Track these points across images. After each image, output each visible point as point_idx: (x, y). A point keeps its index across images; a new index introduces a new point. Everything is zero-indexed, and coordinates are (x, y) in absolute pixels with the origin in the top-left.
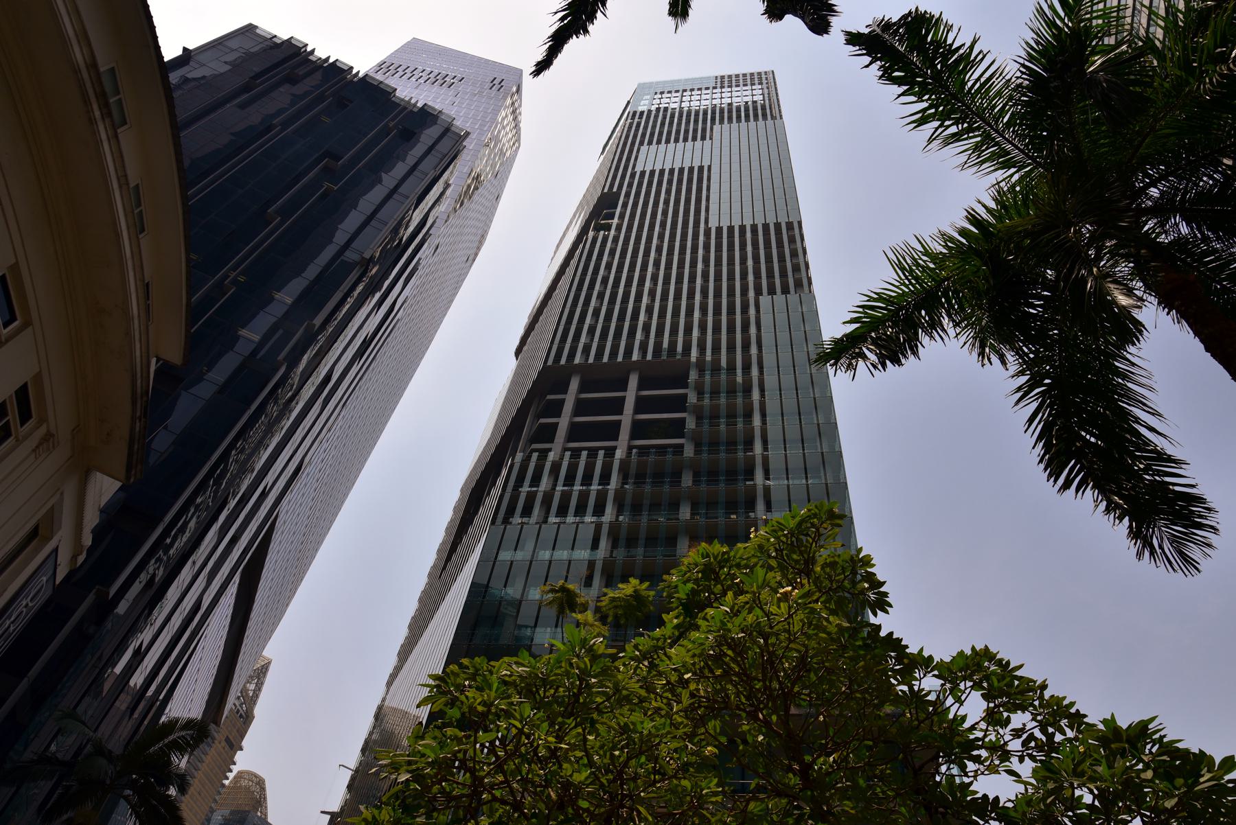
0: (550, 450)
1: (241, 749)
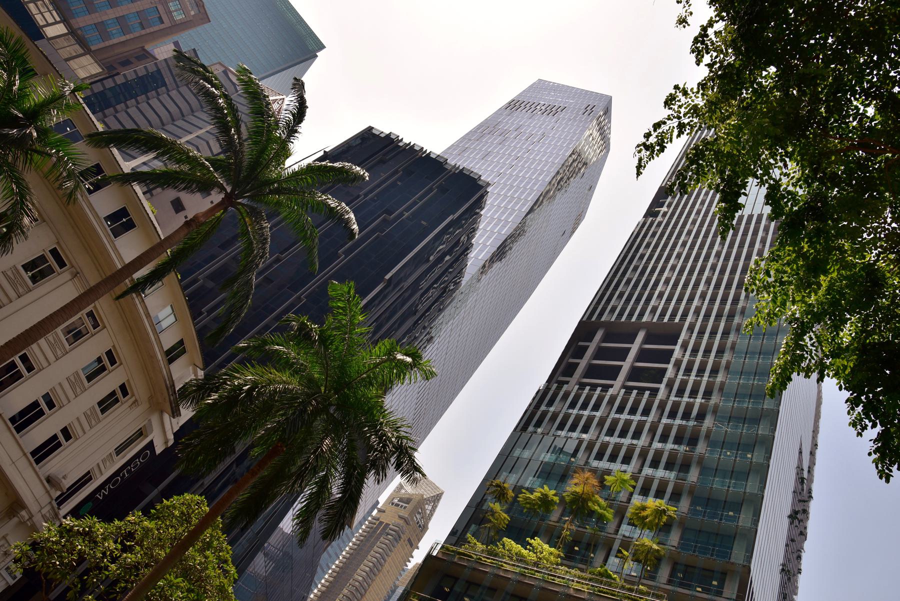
0: (612, 386)
1: (418, 548)
